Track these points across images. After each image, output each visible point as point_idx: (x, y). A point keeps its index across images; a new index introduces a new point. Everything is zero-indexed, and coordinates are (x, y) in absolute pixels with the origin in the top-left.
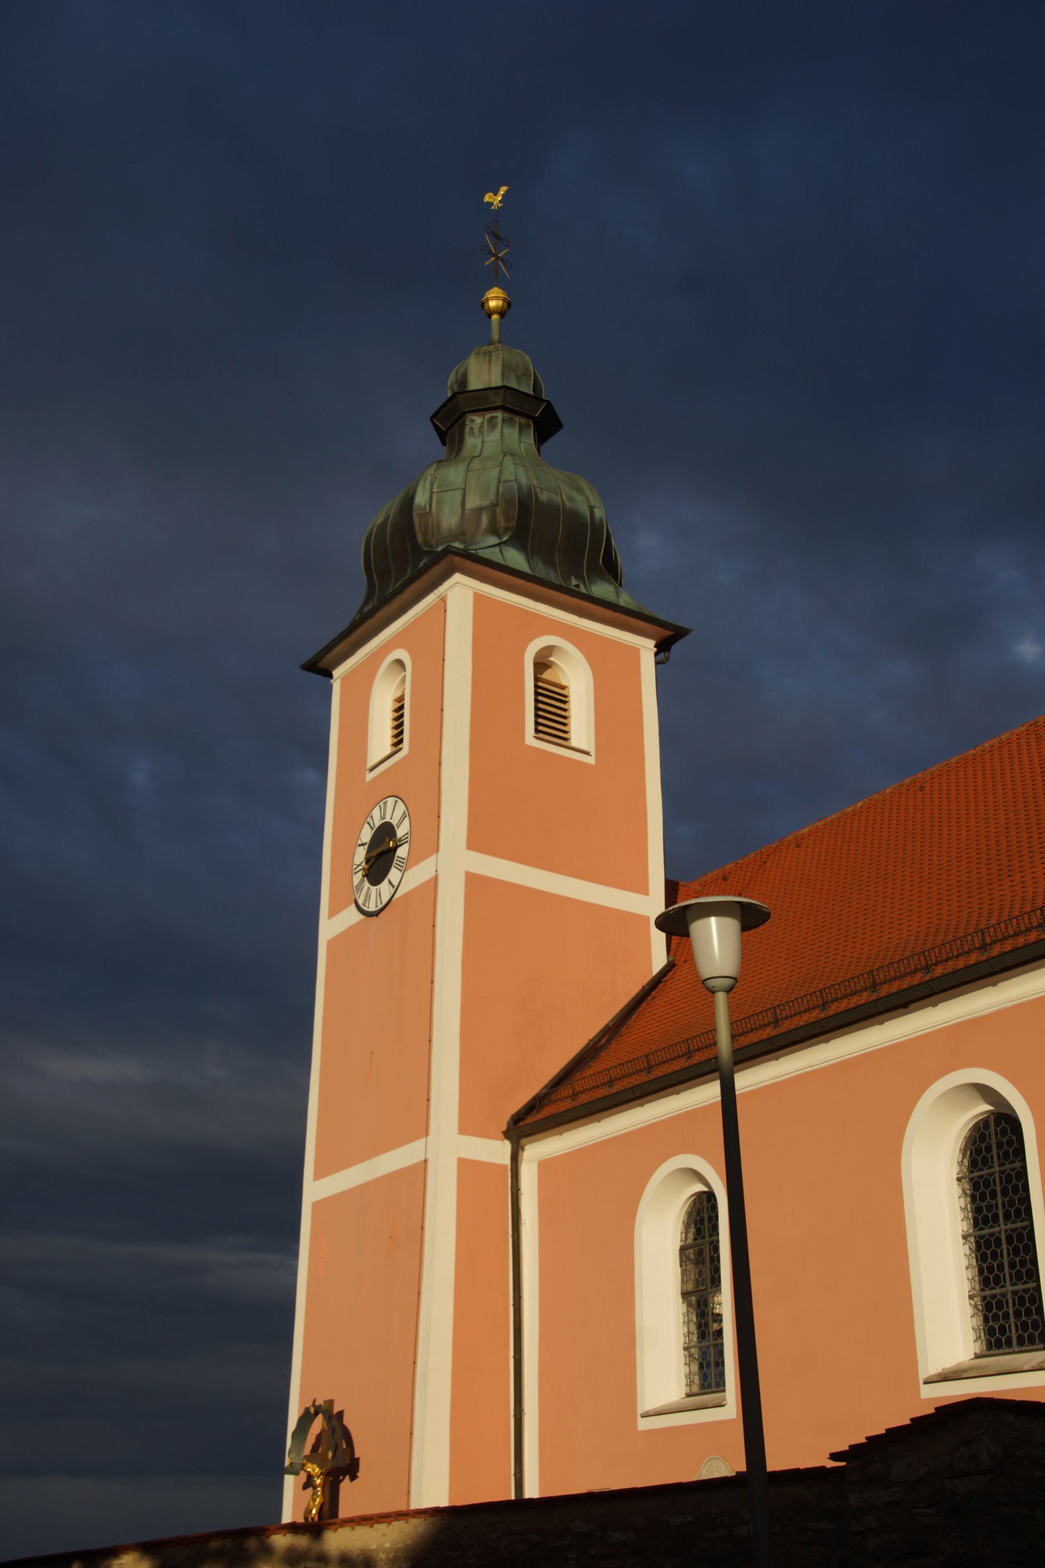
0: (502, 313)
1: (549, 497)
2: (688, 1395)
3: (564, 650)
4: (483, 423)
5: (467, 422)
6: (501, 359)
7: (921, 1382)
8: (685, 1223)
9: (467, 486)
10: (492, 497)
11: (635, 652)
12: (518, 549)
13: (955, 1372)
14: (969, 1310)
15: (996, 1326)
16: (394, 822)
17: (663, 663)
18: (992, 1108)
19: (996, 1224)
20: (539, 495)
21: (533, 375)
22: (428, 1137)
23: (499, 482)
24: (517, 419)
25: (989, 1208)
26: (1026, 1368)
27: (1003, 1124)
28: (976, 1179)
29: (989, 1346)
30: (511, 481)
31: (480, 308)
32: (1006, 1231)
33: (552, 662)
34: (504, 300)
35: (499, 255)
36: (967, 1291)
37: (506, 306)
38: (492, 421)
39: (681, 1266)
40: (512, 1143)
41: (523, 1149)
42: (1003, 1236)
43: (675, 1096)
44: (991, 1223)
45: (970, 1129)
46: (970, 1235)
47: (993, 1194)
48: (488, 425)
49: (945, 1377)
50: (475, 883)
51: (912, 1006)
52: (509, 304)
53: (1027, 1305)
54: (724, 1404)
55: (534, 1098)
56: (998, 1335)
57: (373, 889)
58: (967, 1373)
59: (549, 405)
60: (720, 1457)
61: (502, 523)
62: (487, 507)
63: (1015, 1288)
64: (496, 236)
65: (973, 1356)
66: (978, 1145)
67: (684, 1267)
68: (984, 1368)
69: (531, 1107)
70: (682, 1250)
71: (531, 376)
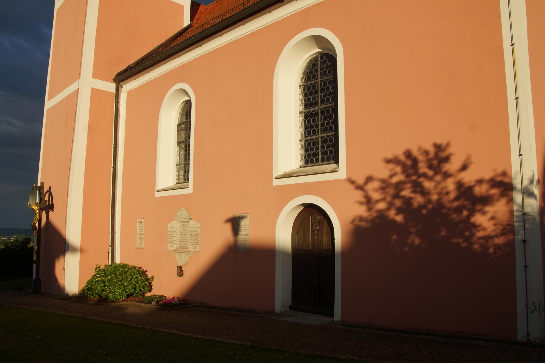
2: (177, 184)
13: (291, 174)
14: (299, 146)
18: (320, 50)
27: (325, 58)
29: (307, 162)
32: (321, 109)
36: (299, 137)
39: (178, 131)
40: (116, 83)
41: (122, 87)
43: (178, 58)
45: (308, 62)
46: (302, 85)
47: (317, 92)
49: (286, 176)
54: (188, 187)
55: (128, 67)
58: (296, 174)
60: (184, 209)
63: (323, 135)
65: (299, 167)
67: (179, 132)
70: (179, 125)
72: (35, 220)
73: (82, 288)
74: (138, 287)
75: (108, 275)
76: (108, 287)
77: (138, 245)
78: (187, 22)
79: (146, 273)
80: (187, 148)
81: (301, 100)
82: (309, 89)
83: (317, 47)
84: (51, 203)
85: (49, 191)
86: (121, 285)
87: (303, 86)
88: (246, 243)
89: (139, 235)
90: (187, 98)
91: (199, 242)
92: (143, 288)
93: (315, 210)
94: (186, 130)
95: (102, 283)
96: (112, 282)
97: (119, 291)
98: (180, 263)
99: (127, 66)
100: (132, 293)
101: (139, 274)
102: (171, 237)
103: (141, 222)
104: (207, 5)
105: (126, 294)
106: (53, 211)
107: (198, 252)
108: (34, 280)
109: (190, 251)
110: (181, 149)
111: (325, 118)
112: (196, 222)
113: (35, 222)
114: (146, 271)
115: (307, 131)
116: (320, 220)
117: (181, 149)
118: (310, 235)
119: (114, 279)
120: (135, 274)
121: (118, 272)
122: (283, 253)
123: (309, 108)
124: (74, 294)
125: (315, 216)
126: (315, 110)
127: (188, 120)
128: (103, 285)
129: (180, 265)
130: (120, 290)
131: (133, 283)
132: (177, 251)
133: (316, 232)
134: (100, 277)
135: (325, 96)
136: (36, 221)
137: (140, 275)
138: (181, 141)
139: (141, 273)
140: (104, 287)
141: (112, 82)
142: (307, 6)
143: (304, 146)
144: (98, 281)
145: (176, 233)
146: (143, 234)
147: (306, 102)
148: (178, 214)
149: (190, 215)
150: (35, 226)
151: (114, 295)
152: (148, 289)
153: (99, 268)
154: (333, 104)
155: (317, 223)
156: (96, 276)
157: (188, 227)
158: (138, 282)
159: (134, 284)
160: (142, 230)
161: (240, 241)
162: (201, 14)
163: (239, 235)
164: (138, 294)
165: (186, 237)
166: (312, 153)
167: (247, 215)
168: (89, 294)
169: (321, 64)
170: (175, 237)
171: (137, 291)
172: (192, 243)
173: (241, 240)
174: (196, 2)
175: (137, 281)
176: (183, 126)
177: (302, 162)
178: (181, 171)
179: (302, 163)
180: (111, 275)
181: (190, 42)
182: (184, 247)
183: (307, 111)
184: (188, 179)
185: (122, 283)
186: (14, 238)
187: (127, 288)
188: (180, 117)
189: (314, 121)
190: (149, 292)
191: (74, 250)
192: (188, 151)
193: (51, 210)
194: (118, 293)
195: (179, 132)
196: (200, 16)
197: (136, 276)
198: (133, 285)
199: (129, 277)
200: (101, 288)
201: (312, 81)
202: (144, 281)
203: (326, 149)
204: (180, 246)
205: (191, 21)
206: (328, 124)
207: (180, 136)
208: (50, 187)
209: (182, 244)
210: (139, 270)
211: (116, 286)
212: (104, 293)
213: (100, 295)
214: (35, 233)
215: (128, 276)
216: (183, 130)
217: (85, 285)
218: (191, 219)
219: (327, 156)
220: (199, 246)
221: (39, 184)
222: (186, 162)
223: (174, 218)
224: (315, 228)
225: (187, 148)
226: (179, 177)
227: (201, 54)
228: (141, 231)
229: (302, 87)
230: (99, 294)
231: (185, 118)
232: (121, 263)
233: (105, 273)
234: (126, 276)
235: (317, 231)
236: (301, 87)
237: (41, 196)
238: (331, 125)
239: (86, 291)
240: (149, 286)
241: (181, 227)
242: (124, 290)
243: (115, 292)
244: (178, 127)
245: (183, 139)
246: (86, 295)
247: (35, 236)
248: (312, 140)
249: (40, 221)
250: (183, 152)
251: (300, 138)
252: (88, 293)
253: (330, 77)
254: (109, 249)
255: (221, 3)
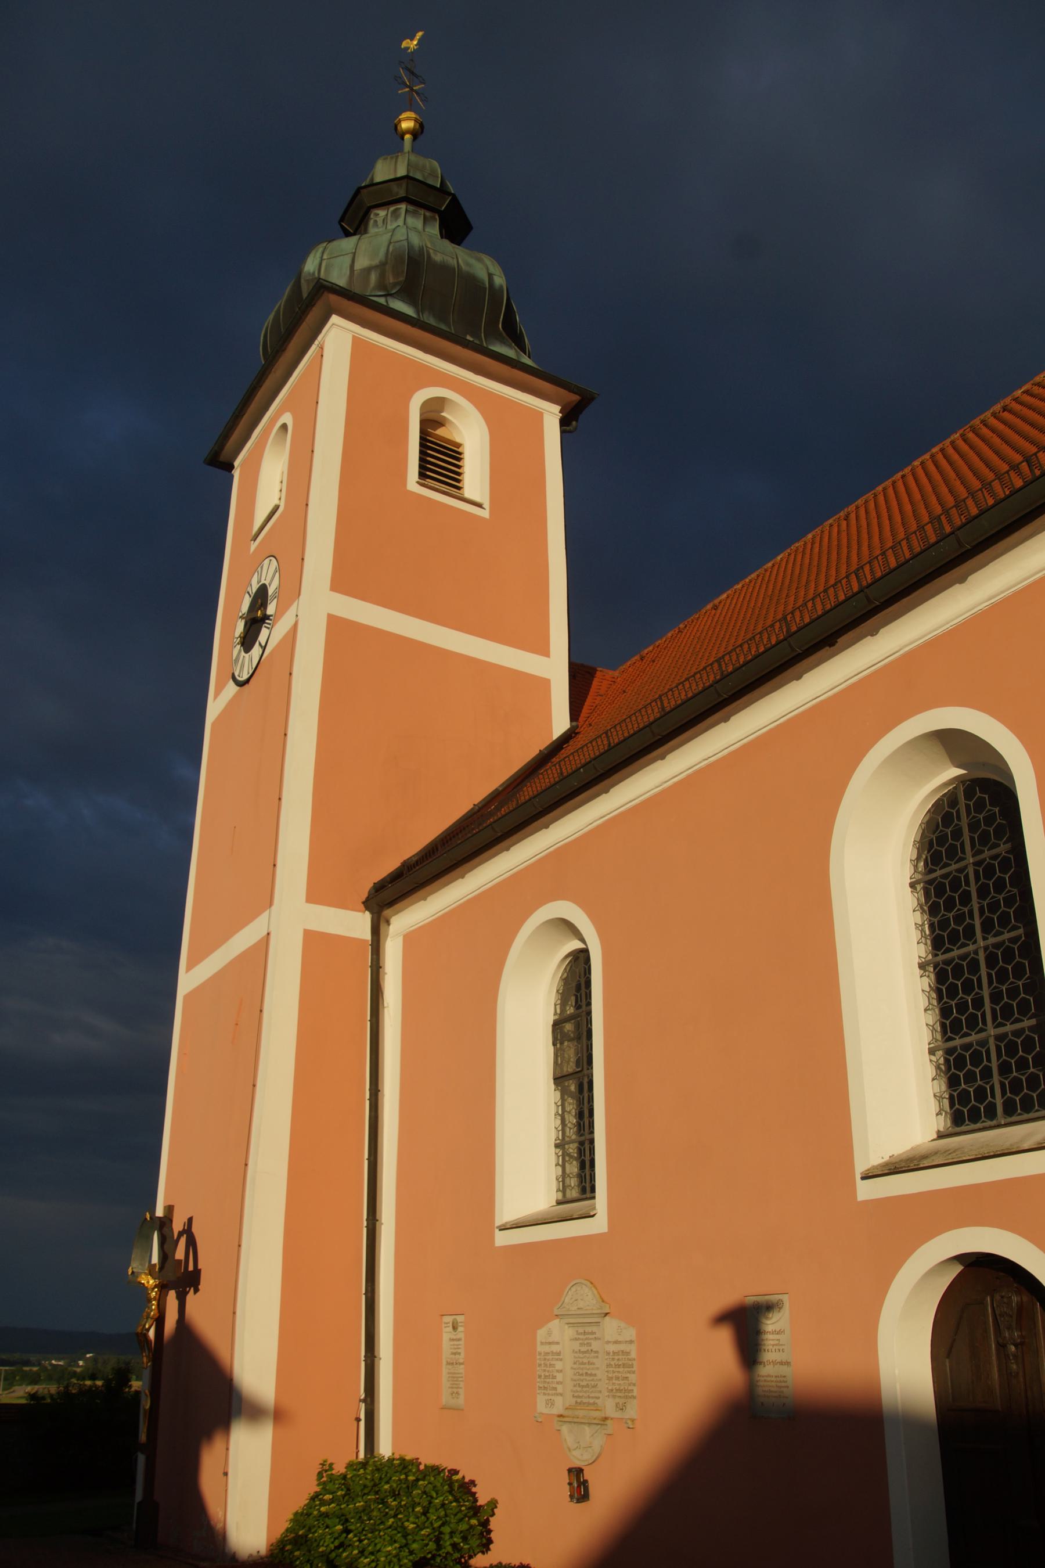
0: (415, 134)
1: (443, 259)
2: (559, 1203)
3: (456, 403)
4: (387, 215)
5: (372, 216)
6: (406, 162)
7: (858, 1177)
8: (561, 991)
9: (357, 251)
10: (381, 255)
11: (539, 416)
12: (406, 303)
13: (910, 1160)
14: (930, 1071)
15: (971, 1090)
16: (267, 583)
17: (570, 432)
18: (961, 772)
19: (970, 940)
20: (432, 255)
21: (440, 176)
22: (274, 908)
23: (390, 243)
24: (422, 211)
25: (959, 918)
26: (1026, 1146)
27: (978, 794)
28: (939, 879)
29: (957, 1119)
30: (402, 241)
31: (394, 131)
32: (986, 948)
33: (445, 418)
34: (416, 120)
35: (414, 88)
37: (418, 126)
38: (395, 214)
39: (554, 1044)
40: (372, 913)
41: (388, 923)
42: (982, 957)
44: (962, 940)
45: (929, 811)
46: (918, 882)
47: (966, 899)
48: (391, 216)
50: (337, 626)
51: (841, 640)
52: (421, 125)
53: (1021, 1053)
54: (592, 1214)
56: (973, 1102)
57: (247, 656)
59: (455, 199)
61: (391, 279)
62: (376, 267)
63: (1001, 1030)
64: (412, 73)
65: (935, 1136)
66: (941, 831)
67: (558, 1045)
68: (954, 1152)
69: (396, 876)
70: (557, 1025)
71: (438, 177)
72: (147, 1318)
73: (278, 1536)
74: (447, 1537)
75: (358, 1496)
76: (355, 1536)
77: (446, 1399)
78: (560, 723)
79: (474, 1490)
80: (586, 1095)
81: (920, 926)
82: (940, 890)
83: (950, 764)
84: (191, 1268)
85: (188, 1231)
86: (396, 1529)
87: (922, 885)
88: (785, 1390)
89: (450, 1367)
90: (576, 945)
91: (635, 1389)
92: (465, 1539)
93: (1002, 1274)
94: (578, 1038)
95: (337, 1520)
96: (369, 1519)
97: (390, 1548)
98: (579, 1459)
99: (402, 861)
100: (429, 1556)
101: (451, 1492)
102: (547, 1374)
103: (453, 1323)
104: (615, 670)
105: (410, 1560)
106: (196, 1291)
107: (633, 1420)
108: (139, 1503)
109: (606, 1419)
110: (566, 1097)
111: (1002, 976)
112: (623, 1325)
113: (147, 1326)
114: (473, 1483)
115: (948, 1022)
116: (1021, 1307)
117: (566, 1097)
118: (994, 1358)
119: (373, 1510)
120: (437, 1494)
121: (387, 1487)
122: (909, 1422)
123: (948, 950)
124: (255, 1553)
125: (1003, 1294)
126: (967, 955)
127: (584, 1008)
128: (340, 1527)
129: (578, 1464)
130: (391, 1545)
131: (431, 1523)
132: (568, 1417)
133: (1013, 1348)
134: (332, 1501)
135: (994, 907)
136: (150, 1321)
137: (452, 1495)
138: (565, 1073)
139: (456, 1489)
140: (344, 1535)
141: (359, 911)
142: (907, 649)
143: (943, 1067)
144: (326, 1515)
145: (561, 1360)
146: (461, 1364)
147: (937, 931)
148: (567, 1300)
149: (603, 1301)
150: (146, 1336)
151: (373, 1561)
152: (478, 1542)
153: (329, 1473)
154: (1021, 931)
155: (1011, 1316)
156: (321, 1497)
157: (600, 1339)
158: (448, 1519)
159: (436, 1525)
160: (459, 1351)
161: (766, 1384)
162: (599, 698)
163: (761, 1363)
164: (449, 1558)
165: (594, 1372)
166: (971, 1089)
167: (780, 1297)
168: (299, 1558)
169: (968, 813)
170: (558, 1371)
171: (445, 1548)
172: (612, 1390)
173: (769, 1379)
174: (582, 665)
175: (446, 1515)
176: (569, 1027)
177: (942, 1118)
178: (572, 1163)
179: (942, 1123)
180: (365, 1494)
181: (576, 784)
182: (589, 1404)
183: (940, 958)
184: (593, 1189)
185: (400, 1524)
186: (86, 1360)
187: (414, 1541)
188: (559, 1002)
189: (968, 987)
190: (483, 1553)
191: (254, 1412)
192: (589, 1102)
193: (192, 1289)
194: (386, 1557)
195: (558, 1045)
196: (597, 702)
197: (442, 1498)
198: (434, 1529)
199: (419, 1504)
200: (335, 1539)
201: (946, 865)
202: (466, 1516)
203: (1015, 1074)
204: (576, 1402)
205: (572, 720)
206: (1013, 993)
207: (563, 1058)
208: (190, 1220)
209: (581, 1394)
210: (450, 1478)
211: (380, 1531)
212: (345, 1554)
213: (333, 1560)
214: (145, 1360)
215: (417, 1500)
216: (569, 1041)
217: (287, 1525)
218: (606, 1314)
219: (1022, 1094)
220: (635, 1401)
221: (160, 1212)
222: (582, 1135)
223: (556, 1312)
224: (1007, 1335)
225: (586, 1095)
226: (563, 1181)
227: (609, 814)
228: (455, 1354)
229: (919, 887)
230: (328, 1558)
231: (574, 1004)
232: (397, 1456)
233: (348, 1489)
234: (410, 1499)
235: (1016, 1345)
236: (916, 889)
237: (166, 1247)
238: (1022, 995)
239: (288, 1547)
240: (482, 1533)
241: (576, 1339)
242: (406, 1545)
243: (379, 1551)
244: (554, 1031)
245: (571, 1067)
246: (288, 1561)
247: (146, 1369)
248: (966, 1047)
249: (160, 1321)
250: (571, 1106)
251: (929, 1044)
252: (297, 1553)
253: (1003, 848)
254: (359, 1410)
255: (654, 661)
